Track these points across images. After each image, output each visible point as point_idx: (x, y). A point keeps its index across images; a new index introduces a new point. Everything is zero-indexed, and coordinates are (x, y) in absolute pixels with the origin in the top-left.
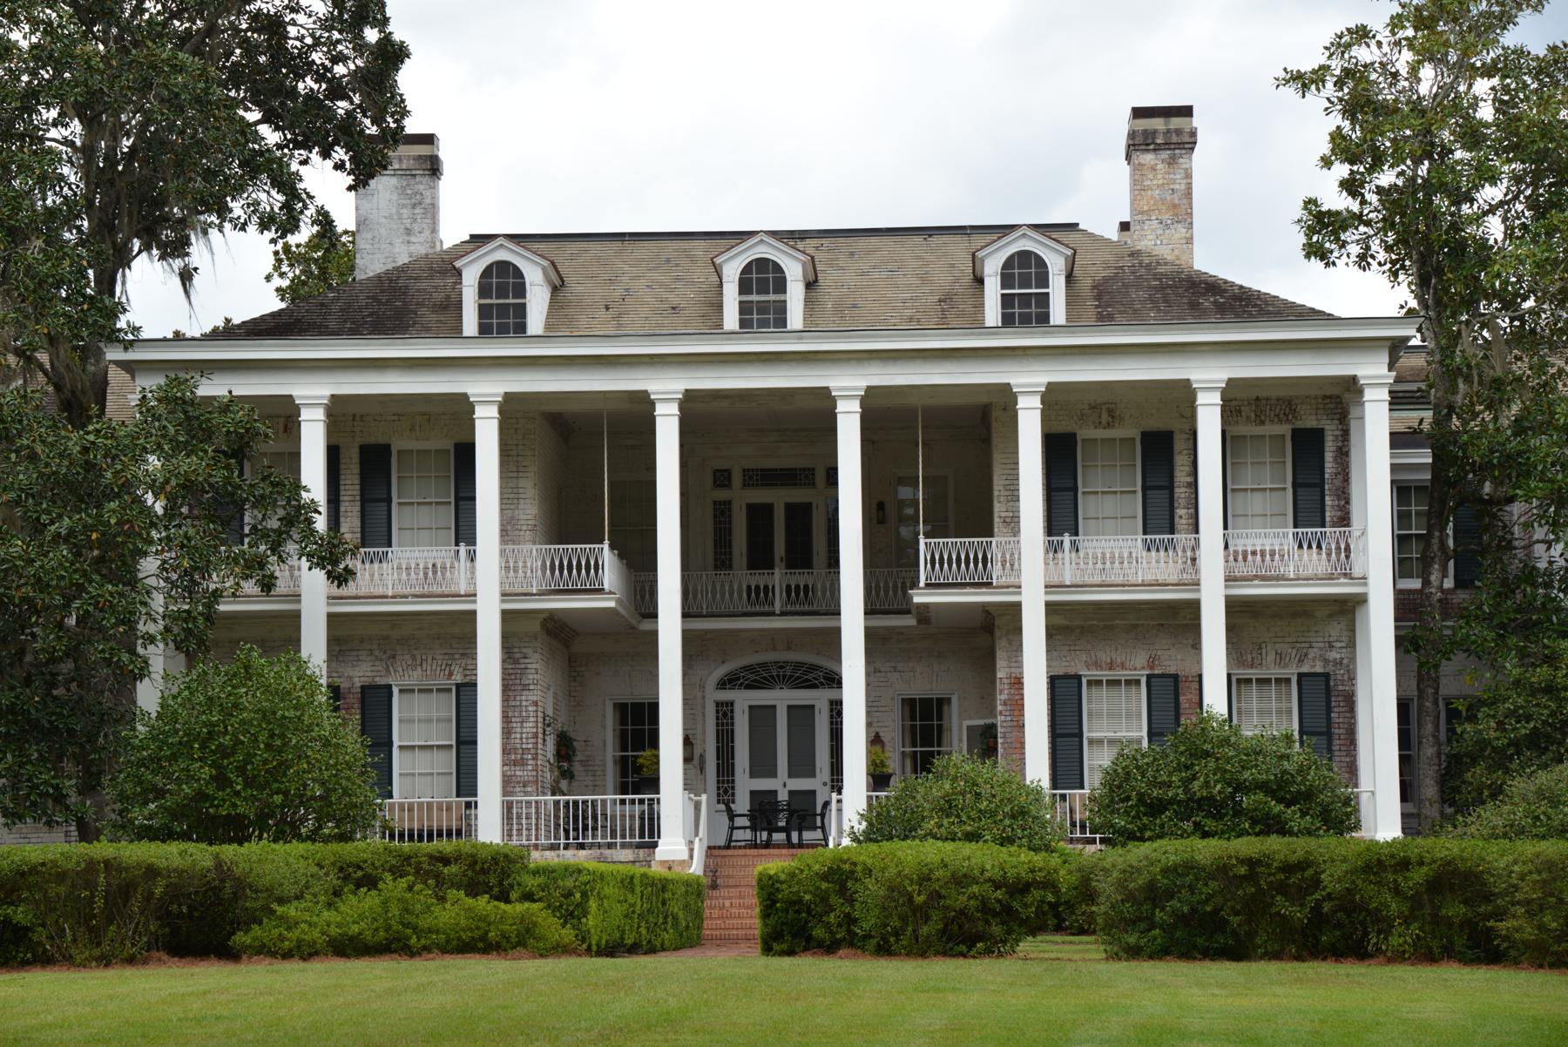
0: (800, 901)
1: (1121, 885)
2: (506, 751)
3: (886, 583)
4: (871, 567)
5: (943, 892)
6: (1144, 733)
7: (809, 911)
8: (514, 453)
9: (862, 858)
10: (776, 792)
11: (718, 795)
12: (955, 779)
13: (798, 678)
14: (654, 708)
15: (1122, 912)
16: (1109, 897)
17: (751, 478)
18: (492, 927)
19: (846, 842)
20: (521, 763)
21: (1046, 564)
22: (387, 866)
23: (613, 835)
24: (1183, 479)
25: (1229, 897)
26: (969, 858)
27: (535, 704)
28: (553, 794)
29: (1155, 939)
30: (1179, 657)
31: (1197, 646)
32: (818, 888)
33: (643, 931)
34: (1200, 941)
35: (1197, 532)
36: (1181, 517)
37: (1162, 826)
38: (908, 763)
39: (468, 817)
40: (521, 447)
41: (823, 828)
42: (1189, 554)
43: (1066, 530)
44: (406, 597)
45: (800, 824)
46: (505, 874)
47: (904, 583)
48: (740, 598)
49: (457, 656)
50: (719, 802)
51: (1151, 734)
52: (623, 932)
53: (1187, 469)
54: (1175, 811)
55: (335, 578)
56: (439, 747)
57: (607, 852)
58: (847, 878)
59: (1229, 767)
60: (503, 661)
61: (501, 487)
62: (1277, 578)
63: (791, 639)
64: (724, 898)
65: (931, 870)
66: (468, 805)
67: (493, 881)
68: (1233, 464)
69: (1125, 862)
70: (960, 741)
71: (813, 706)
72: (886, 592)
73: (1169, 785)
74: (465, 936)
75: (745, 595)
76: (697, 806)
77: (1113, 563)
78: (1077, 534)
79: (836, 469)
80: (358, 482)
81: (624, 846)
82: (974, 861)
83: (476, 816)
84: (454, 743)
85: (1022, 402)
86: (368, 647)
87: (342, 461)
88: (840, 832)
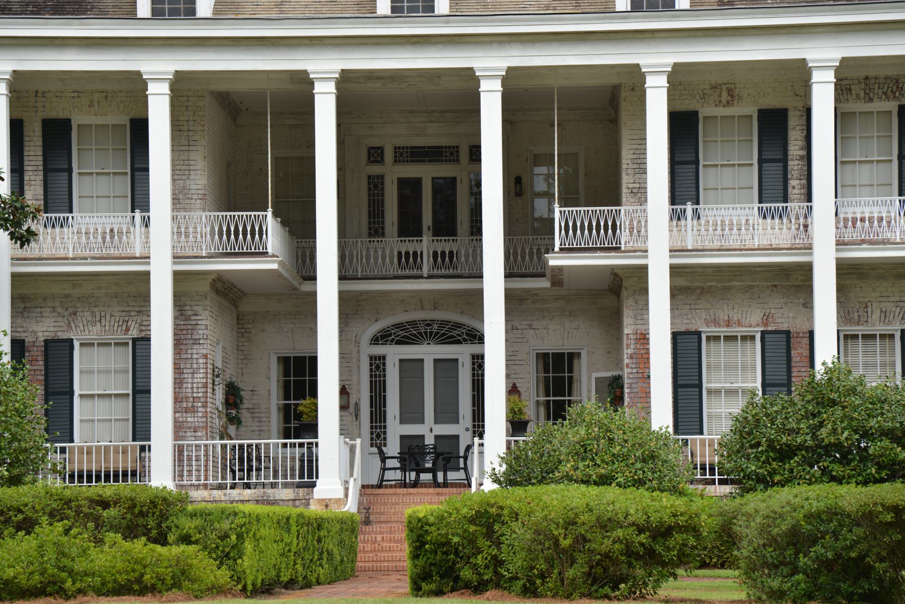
0: (448, 543)
1: (763, 530)
2: (178, 399)
3: (523, 249)
4: (510, 235)
5: (589, 536)
6: (758, 384)
7: (457, 553)
8: (186, 128)
9: (508, 502)
10: (423, 437)
11: (372, 439)
12: (589, 426)
13: (444, 334)
14: (314, 360)
15: (764, 556)
16: (750, 542)
17: (401, 154)
18: (148, 570)
19: (489, 486)
20: (193, 410)
21: (671, 231)
22: (48, 510)
23: (275, 476)
24: (796, 153)
25: (873, 543)
26: (613, 503)
27: (205, 356)
28: (222, 438)
29: (799, 583)
30: (791, 315)
31: (808, 305)
32: (466, 531)
33: (299, 567)
34: (844, 586)
35: (809, 199)
36: (794, 187)
37: (791, 471)
38: (542, 410)
39: (142, 459)
40: (191, 123)
41: (465, 469)
42: (802, 221)
43: (689, 200)
44: (85, 259)
45: (445, 465)
46: (164, 517)
47: (539, 250)
48: (392, 263)
49: (133, 313)
50: (372, 446)
51: (764, 385)
52: (279, 570)
53: (800, 143)
54: (803, 456)
55: (17, 239)
56: (117, 395)
57: (270, 491)
58: (495, 521)
59: (856, 415)
60: (176, 318)
61: (173, 161)
62: (885, 242)
63: (438, 300)
64: (376, 533)
65: (576, 514)
66: (143, 449)
67: (152, 523)
68: (842, 138)
69: (768, 507)
70: (589, 391)
71: (457, 360)
72: (523, 258)
73: (797, 432)
74: (122, 578)
75: (396, 260)
76: (352, 449)
77: (731, 229)
78: (698, 203)
79: (479, 147)
80: (40, 153)
81: (286, 485)
82: (617, 506)
83: (149, 457)
84: (130, 392)
85: (650, 81)
86: (51, 305)
87: (26, 134)
88: (482, 473)
